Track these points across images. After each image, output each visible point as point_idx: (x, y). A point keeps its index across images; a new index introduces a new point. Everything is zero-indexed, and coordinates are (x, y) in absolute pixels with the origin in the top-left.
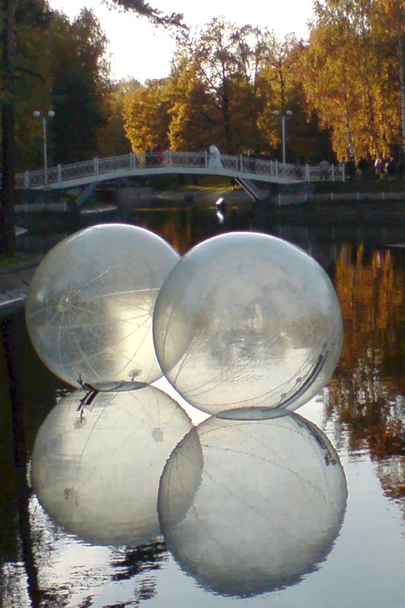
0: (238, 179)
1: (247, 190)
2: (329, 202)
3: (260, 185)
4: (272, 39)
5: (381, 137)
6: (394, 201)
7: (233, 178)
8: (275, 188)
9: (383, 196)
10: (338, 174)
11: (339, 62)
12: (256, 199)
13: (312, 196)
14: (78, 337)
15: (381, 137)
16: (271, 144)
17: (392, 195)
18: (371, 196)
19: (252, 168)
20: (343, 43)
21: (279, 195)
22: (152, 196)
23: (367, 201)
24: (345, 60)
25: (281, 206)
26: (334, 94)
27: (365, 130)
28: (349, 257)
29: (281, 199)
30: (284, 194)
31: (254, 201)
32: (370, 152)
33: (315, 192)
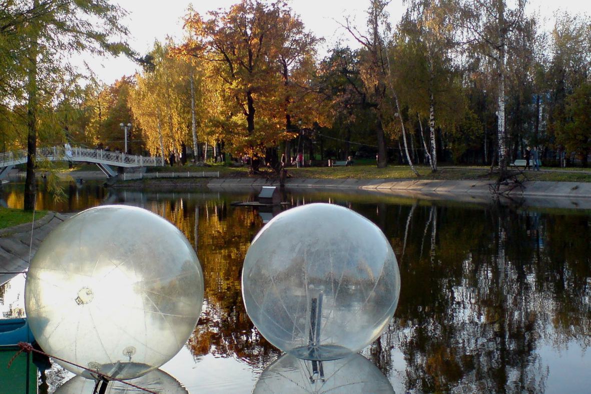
0: (99, 164)
1: (413, 149)
2: (156, 178)
3: (112, 167)
4: (543, 34)
5: (177, 140)
6: (196, 177)
7: (95, 163)
8: (121, 170)
9: (189, 174)
10: (152, 161)
11: (155, 96)
12: (110, 176)
13: (145, 174)
14: (310, 240)
15: (177, 140)
16: (94, 144)
17: (194, 174)
18: (182, 174)
19: (108, 157)
20: (157, 84)
21: (125, 174)
22: (17, 175)
23: (179, 178)
24: (158, 95)
25: (126, 180)
26: (151, 115)
27: (168, 136)
28: (435, 199)
29: (125, 176)
30: (127, 173)
31: (108, 177)
32: (170, 149)
33: (146, 172)
